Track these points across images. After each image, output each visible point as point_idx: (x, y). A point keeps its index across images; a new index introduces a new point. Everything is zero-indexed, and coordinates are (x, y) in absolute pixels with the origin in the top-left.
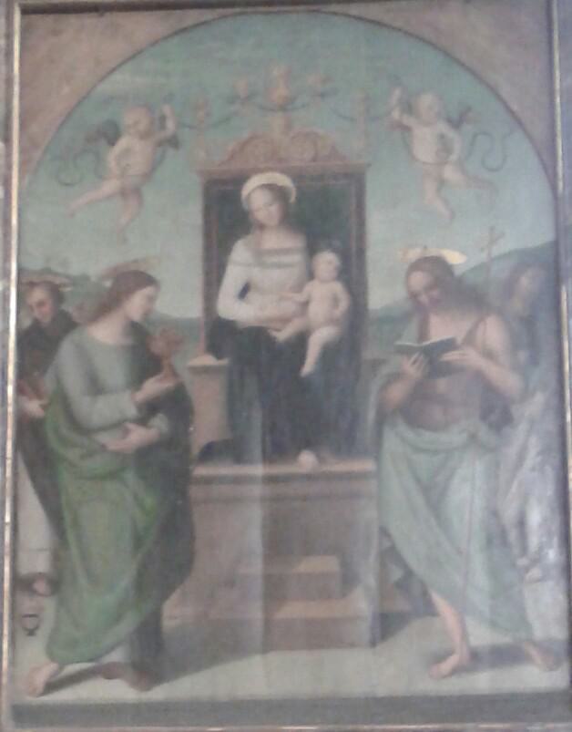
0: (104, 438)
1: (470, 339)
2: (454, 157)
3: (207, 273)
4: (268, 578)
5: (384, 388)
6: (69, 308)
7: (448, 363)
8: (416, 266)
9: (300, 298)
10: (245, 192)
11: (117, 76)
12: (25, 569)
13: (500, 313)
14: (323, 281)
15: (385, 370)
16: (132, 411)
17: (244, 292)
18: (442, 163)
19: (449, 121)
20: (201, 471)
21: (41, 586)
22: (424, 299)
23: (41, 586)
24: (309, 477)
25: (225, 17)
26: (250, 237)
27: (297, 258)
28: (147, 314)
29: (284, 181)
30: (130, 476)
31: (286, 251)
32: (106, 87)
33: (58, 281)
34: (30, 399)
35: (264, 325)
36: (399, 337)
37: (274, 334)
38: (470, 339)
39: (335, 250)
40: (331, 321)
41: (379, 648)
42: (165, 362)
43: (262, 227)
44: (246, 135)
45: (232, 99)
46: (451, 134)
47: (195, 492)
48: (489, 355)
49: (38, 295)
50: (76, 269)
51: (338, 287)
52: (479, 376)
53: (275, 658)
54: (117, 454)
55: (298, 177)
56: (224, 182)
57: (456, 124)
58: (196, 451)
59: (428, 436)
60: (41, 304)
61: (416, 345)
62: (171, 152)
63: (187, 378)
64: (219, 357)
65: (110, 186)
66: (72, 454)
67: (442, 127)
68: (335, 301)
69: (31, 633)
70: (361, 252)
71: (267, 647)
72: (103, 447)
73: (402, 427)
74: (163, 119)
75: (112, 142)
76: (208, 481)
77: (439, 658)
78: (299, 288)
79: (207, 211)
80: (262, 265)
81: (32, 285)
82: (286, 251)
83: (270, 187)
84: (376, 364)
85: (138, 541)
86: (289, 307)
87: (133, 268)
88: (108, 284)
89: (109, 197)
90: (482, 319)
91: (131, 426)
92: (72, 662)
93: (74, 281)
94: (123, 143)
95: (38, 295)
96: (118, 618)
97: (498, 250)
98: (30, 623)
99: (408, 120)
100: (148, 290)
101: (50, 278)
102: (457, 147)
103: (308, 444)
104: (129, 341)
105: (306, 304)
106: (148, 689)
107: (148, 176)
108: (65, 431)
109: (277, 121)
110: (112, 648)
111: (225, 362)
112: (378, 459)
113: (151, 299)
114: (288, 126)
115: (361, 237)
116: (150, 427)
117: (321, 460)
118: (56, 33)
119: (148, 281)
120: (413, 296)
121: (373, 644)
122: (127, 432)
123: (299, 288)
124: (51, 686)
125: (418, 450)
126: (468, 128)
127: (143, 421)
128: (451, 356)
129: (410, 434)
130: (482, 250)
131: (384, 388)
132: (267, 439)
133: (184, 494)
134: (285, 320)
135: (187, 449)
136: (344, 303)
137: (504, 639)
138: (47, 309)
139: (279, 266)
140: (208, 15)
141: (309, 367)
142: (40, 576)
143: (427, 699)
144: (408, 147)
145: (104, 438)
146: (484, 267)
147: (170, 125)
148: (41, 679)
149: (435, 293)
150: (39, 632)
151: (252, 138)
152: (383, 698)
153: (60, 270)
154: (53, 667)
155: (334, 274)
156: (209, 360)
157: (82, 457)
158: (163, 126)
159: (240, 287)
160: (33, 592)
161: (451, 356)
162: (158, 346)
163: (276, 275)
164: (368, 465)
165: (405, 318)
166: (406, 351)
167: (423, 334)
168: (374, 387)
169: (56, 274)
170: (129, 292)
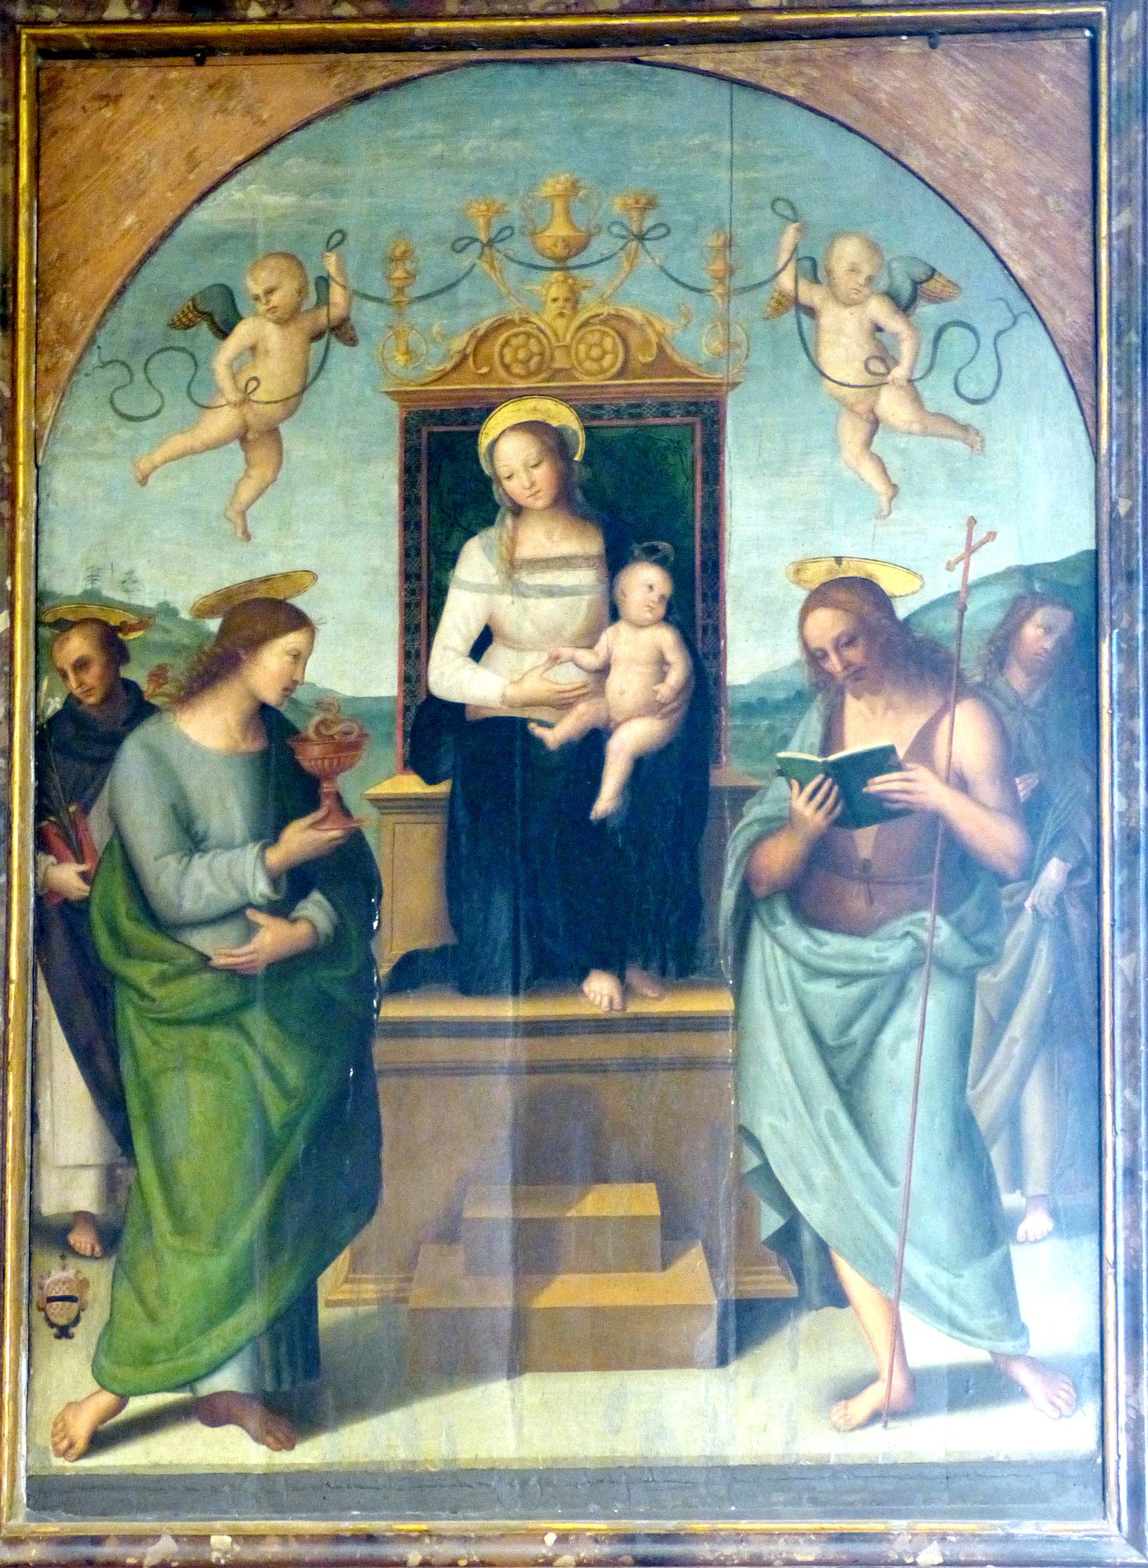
0: (203, 940)
1: (923, 748)
2: (899, 373)
3: (408, 607)
4: (521, 1227)
5: (754, 845)
6: (136, 672)
7: (879, 799)
8: (819, 597)
9: (590, 659)
10: (484, 441)
11: (231, 192)
12: (50, 1206)
13: (983, 693)
14: (640, 626)
15: (754, 811)
16: (261, 888)
17: (481, 647)
18: (875, 386)
19: (891, 296)
20: (392, 1010)
21: (82, 1239)
22: (834, 664)
23: (82, 1239)
24: (602, 1026)
25: (450, 68)
26: (492, 532)
27: (587, 577)
28: (289, 689)
29: (563, 417)
30: (257, 1020)
31: (566, 562)
32: (207, 216)
33: (114, 621)
34: (60, 860)
35: (517, 713)
36: (785, 742)
37: (539, 731)
38: (923, 748)
39: (662, 562)
40: (652, 708)
41: (732, 1367)
42: (326, 787)
43: (518, 511)
44: (487, 317)
45: (460, 245)
46: (894, 323)
47: (383, 1051)
48: (961, 783)
49: (77, 645)
50: (147, 598)
51: (666, 638)
52: (935, 820)
53: (529, 1382)
54: (233, 974)
55: (589, 412)
56: (441, 417)
57: (904, 306)
58: (384, 969)
59: (836, 944)
60: (81, 665)
61: (820, 760)
62: (339, 350)
63: (366, 817)
64: (431, 780)
65: (221, 421)
66: (141, 973)
67: (879, 309)
68: (662, 664)
69: (64, 1332)
70: (714, 566)
71: (516, 1367)
72: (204, 960)
73: (788, 928)
74: (324, 282)
75: (223, 332)
76: (407, 1029)
77: (848, 1391)
78: (589, 638)
79: (409, 473)
80: (518, 591)
81: (63, 626)
82: (566, 562)
83: (534, 428)
84: (744, 795)
85: (271, 1149)
86: (568, 677)
87: (261, 593)
88: (214, 625)
89: (217, 444)
90: (947, 708)
91: (260, 918)
92: (141, 1392)
93: (145, 619)
94: (242, 333)
95: (77, 645)
96: (233, 1300)
97: (985, 564)
98: (61, 1313)
99: (810, 294)
100: (293, 640)
101: (94, 611)
102: (906, 350)
103: (614, 964)
104: (255, 745)
105: (603, 672)
106: (288, 1444)
107: (292, 403)
108: (128, 927)
109: (552, 287)
110: (215, 1368)
111: (443, 788)
112: (738, 991)
113: (299, 658)
114: (573, 300)
115: (714, 535)
116: (294, 921)
117: (627, 990)
118: (109, 99)
119: (299, 621)
120: (814, 657)
121: (722, 1360)
122: (252, 929)
123: (589, 638)
124: (100, 1441)
125: (818, 973)
126: (926, 311)
127: (281, 908)
128: (879, 784)
129: (801, 942)
130: (950, 567)
131: (754, 845)
132: (524, 942)
133: (363, 1061)
134: (563, 704)
135: (370, 963)
136: (677, 673)
137: (975, 1354)
138: (92, 676)
139: (550, 592)
140: (107, 785)
141: (606, 801)
142: (83, 1217)
143: (823, 1469)
144: (809, 348)
145: (203, 940)
146: (956, 601)
147: (337, 295)
148: (81, 1428)
149: (854, 654)
150: (78, 1331)
151: (502, 324)
152: (743, 1468)
153: (119, 596)
154: (106, 1399)
155: (661, 611)
156: (412, 785)
157: (163, 979)
158: (323, 300)
159: (475, 632)
160: (68, 1250)
161: (879, 784)
162: (312, 756)
163: (547, 608)
164: (719, 1003)
165: (799, 700)
166: (787, 769)
167: (831, 737)
168: (735, 847)
169: (109, 604)
170: (256, 643)
